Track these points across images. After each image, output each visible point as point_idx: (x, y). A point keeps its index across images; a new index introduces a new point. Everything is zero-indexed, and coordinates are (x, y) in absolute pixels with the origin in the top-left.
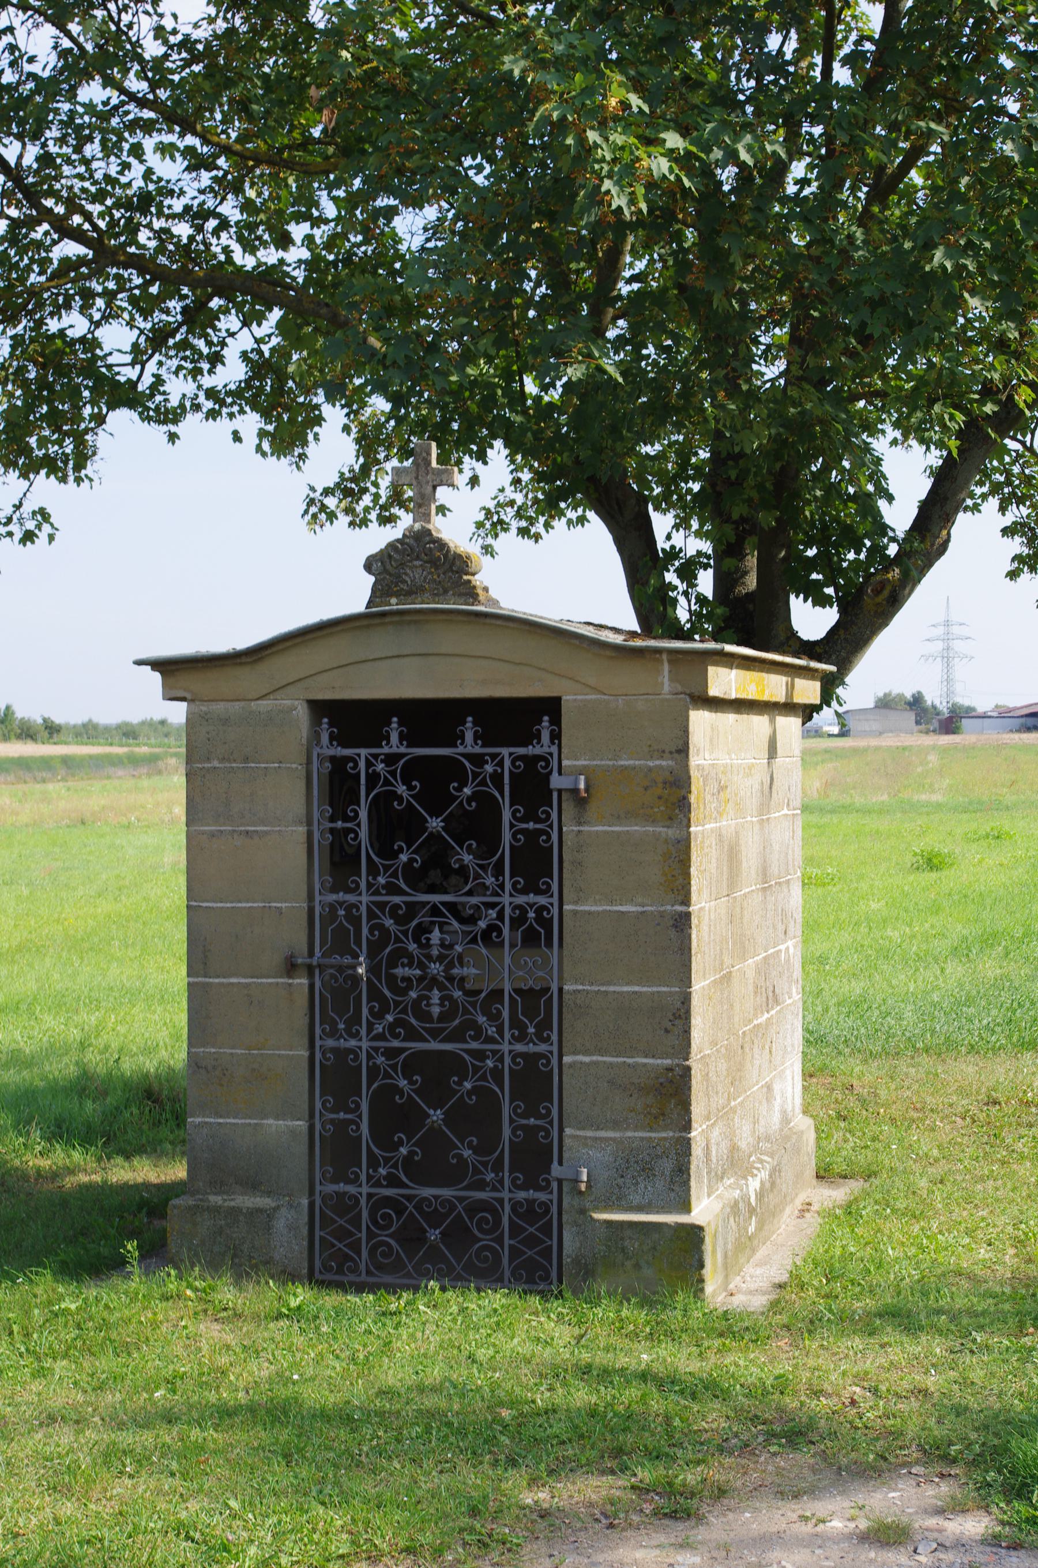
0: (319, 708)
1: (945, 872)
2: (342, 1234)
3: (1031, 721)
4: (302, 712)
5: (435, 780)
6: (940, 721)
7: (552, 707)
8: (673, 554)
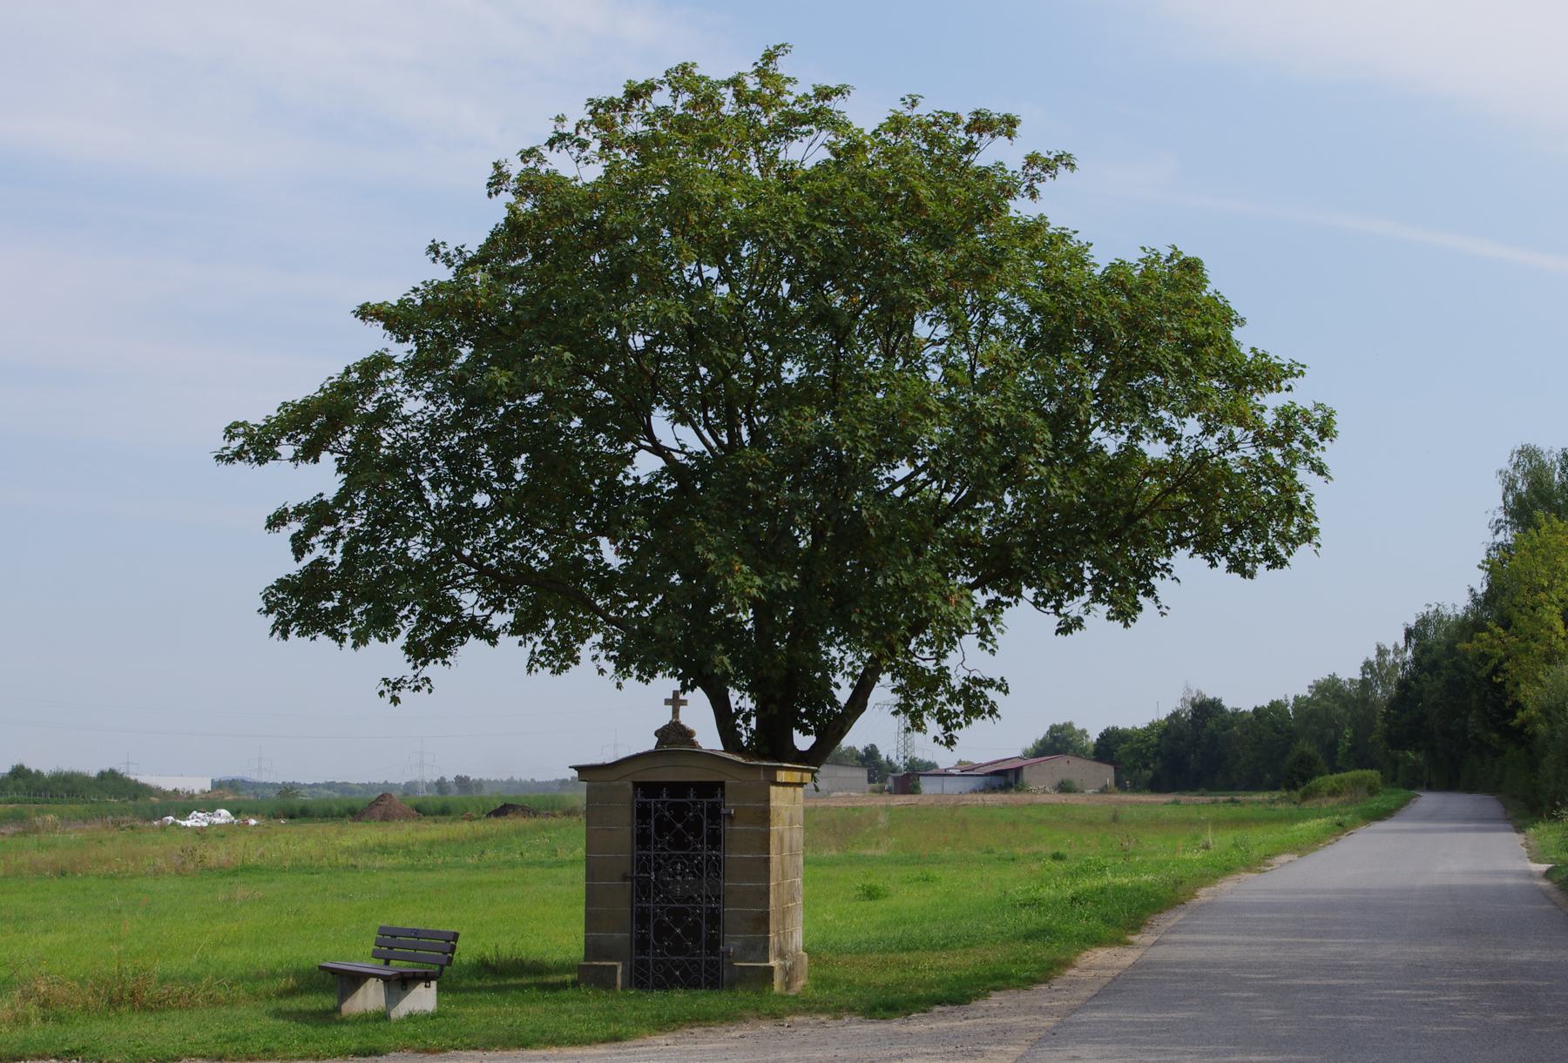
0: (636, 785)
1: (878, 903)
2: (642, 974)
3: (997, 781)
4: (630, 786)
5: (679, 811)
6: (895, 779)
7: (721, 784)
8: (740, 711)
